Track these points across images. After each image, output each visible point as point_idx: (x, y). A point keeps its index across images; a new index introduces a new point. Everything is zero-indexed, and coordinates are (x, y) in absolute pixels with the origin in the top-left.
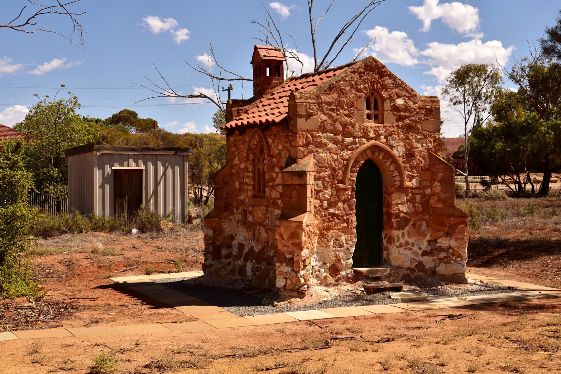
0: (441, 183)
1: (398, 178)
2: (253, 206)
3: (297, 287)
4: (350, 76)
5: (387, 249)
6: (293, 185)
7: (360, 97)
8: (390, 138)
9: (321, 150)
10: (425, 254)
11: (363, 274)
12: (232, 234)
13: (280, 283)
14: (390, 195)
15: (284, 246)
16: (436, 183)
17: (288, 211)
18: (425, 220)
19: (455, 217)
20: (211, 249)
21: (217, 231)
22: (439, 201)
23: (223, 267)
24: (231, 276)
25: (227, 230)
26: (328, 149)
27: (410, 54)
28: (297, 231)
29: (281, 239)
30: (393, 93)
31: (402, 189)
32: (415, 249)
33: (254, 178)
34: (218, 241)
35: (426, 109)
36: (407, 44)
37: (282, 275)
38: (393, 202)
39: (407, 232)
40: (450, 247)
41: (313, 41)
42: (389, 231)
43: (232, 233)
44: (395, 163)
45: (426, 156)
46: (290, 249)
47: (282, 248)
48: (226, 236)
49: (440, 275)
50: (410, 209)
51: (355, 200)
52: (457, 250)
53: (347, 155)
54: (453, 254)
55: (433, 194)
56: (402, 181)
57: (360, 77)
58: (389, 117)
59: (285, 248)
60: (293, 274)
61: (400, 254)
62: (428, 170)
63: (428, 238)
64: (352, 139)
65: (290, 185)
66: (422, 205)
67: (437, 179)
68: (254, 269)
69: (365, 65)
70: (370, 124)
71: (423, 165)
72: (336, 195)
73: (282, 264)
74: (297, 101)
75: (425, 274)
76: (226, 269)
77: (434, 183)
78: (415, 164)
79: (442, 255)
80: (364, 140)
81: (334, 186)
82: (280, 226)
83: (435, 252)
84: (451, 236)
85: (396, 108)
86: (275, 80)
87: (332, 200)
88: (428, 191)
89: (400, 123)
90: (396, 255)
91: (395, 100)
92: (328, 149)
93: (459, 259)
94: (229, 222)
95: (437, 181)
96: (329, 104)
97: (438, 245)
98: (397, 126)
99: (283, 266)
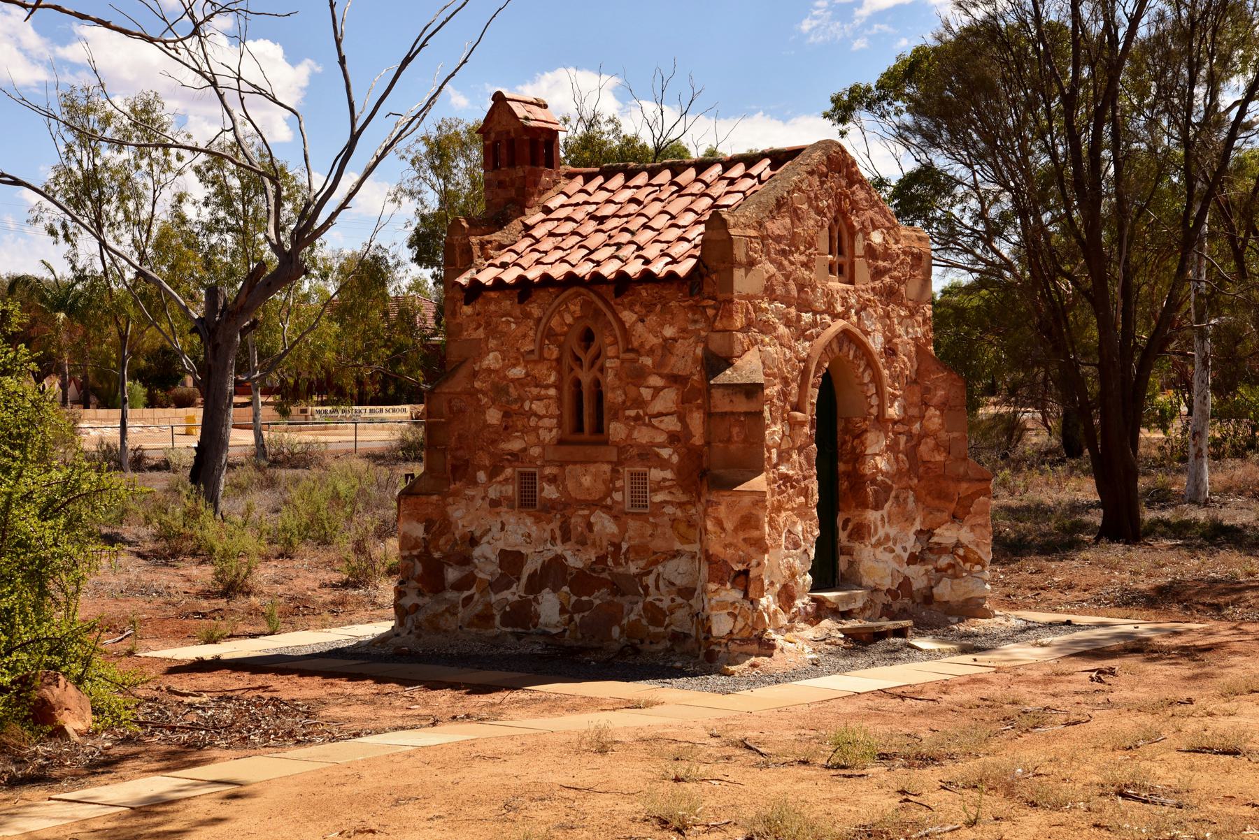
0: (942, 411)
1: (874, 401)
2: (562, 464)
3: (755, 633)
5: (849, 552)
6: (732, 413)
7: (822, 226)
8: (863, 314)
9: (767, 340)
10: (913, 559)
11: (827, 604)
12: (472, 532)
13: (721, 625)
14: (860, 435)
15: (726, 546)
16: (932, 411)
17: (722, 471)
18: (911, 488)
19: (970, 480)
20: (419, 569)
21: (437, 525)
22: (937, 447)
23: (447, 610)
24: (474, 630)
25: (460, 523)
26: (777, 338)
27: (25, 52)
28: (754, 512)
29: (719, 530)
32: (898, 549)
33: (559, 400)
34: (437, 549)
35: (912, 254)
36: (10, 19)
37: (726, 609)
38: (869, 451)
40: (958, 544)
41: (342, 61)
42: (857, 513)
43: (473, 529)
44: (872, 369)
45: (913, 354)
46: (741, 553)
47: (721, 549)
48: (457, 536)
49: (940, 603)
50: (891, 466)
51: (814, 445)
52: (974, 548)
53: (804, 349)
54: (965, 559)
56: (881, 408)
57: (822, 183)
58: (862, 269)
59: (730, 551)
60: (747, 604)
61: (876, 560)
62: (915, 382)
63: (917, 526)
65: (726, 413)
66: (906, 456)
67: (935, 401)
68: (569, 608)
69: (828, 157)
70: (835, 284)
71: (908, 372)
72: (790, 436)
73: (724, 584)
74: (732, 232)
75: (913, 603)
76: (456, 614)
77: (926, 410)
78: (898, 369)
79: (944, 561)
81: (785, 415)
82: (719, 504)
83: (930, 556)
84: (962, 520)
85: (871, 252)
86: (546, 176)
87: (784, 447)
88: (916, 427)
89: (878, 284)
90: (870, 564)
92: (777, 338)
93: (978, 568)
94: (467, 505)
95: (934, 407)
96: (778, 239)
97: (935, 539)
98: (873, 289)
99: (726, 590)
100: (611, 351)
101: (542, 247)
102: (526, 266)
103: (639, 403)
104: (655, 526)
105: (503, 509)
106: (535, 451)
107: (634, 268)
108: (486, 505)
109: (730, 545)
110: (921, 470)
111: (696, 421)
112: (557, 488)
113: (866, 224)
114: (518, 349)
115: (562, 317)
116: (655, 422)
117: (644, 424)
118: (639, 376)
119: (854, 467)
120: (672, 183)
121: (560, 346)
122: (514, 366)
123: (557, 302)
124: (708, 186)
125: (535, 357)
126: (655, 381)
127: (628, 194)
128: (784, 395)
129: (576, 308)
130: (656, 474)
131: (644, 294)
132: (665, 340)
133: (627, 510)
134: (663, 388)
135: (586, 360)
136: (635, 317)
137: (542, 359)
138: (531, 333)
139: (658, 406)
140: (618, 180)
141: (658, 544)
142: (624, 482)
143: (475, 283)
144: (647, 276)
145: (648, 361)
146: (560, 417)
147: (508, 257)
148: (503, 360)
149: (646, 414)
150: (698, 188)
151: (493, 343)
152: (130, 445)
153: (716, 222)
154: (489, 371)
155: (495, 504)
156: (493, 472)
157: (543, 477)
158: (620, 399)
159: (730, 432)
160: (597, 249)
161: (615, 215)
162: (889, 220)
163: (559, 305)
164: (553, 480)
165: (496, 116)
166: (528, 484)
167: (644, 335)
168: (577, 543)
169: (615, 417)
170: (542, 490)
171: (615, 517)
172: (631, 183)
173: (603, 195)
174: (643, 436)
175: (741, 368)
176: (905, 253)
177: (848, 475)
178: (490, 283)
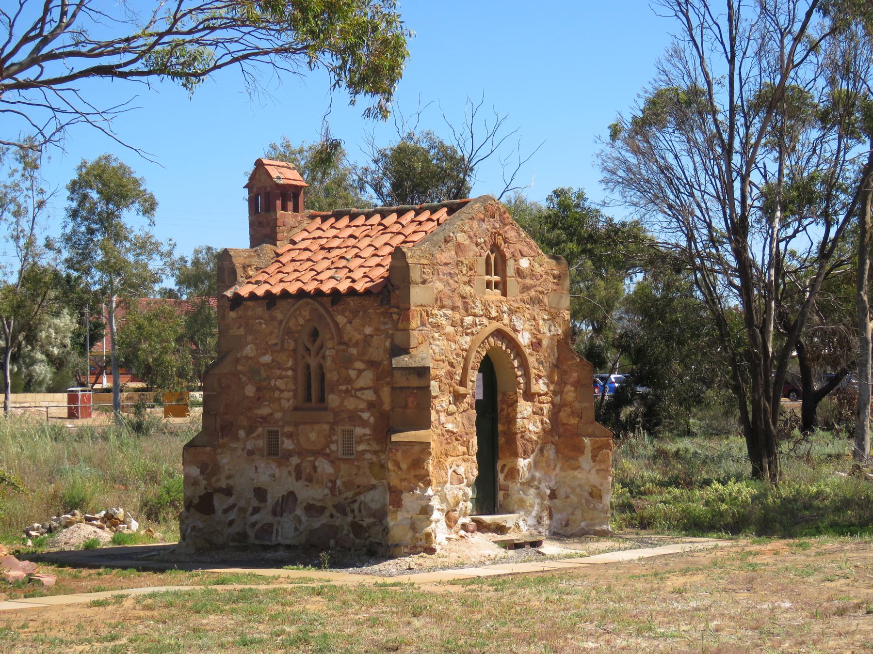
0: (576, 388)
2: (296, 425)
5: (506, 489)
6: (408, 388)
9: (436, 335)
15: (401, 480)
16: (569, 388)
22: (573, 413)
29: (396, 469)
31: (529, 396)
33: (295, 378)
43: (438, 551)
58: (513, 284)
67: (572, 380)
85: (519, 272)
89: (525, 296)
100: (329, 344)
101: (285, 270)
102: (273, 283)
103: (349, 381)
104: (359, 467)
105: (256, 457)
106: (278, 415)
107: (343, 287)
108: (245, 454)
109: (405, 479)
110: (561, 430)
111: (386, 392)
112: (293, 441)
113: (516, 254)
114: (267, 343)
115: (297, 320)
116: (359, 394)
117: (352, 396)
118: (347, 362)
119: (509, 428)
120: (380, 224)
121: (295, 341)
122: (264, 354)
123: (293, 309)
124: (403, 226)
125: (278, 348)
126: (359, 365)
127: (349, 231)
128: (451, 375)
129: (306, 314)
130: (359, 431)
131: (352, 304)
132: (366, 336)
133: (340, 456)
134: (364, 370)
135: (313, 350)
136: (345, 320)
137: (283, 349)
138: (276, 331)
139: (361, 383)
140: (345, 221)
141: (362, 480)
142: (338, 437)
143: (237, 296)
144: (352, 291)
145: (354, 351)
146: (295, 391)
147: (262, 277)
148: (257, 350)
149: (353, 389)
150: (397, 228)
151: (250, 338)
153: (398, 254)
154: (247, 358)
155: (251, 453)
156: (250, 431)
157: (284, 434)
158: (335, 378)
159: (407, 401)
160: (322, 272)
161: (338, 247)
162: (534, 251)
163: (295, 311)
164: (290, 436)
165: (257, 176)
166: (273, 438)
167: (352, 333)
168: (306, 480)
169: (332, 391)
170: (283, 443)
171: (332, 462)
172: (353, 224)
173: (334, 232)
174: (350, 404)
175: (415, 356)
176: (547, 274)
177: (505, 433)
178: (247, 295)
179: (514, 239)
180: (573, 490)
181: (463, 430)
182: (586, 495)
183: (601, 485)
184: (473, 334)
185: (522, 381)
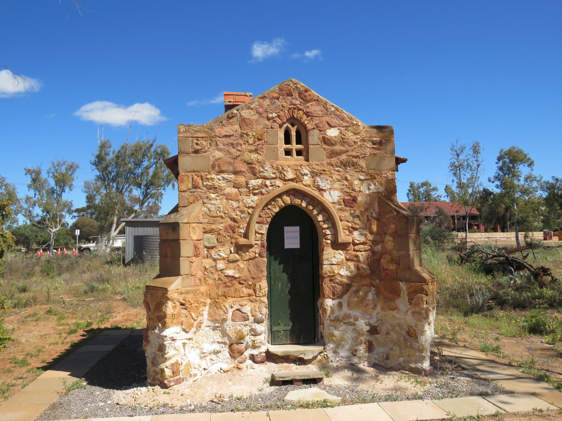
4: (257, 103)
9: (213, 196)
16: (388, 238)
18: (374, 286)
22: (392, 260)
30: (322, 122)
31: (337, 245)
39: (347, 302)
55: (384, 252)
64: (260, 181)
67: (390, 231)
77: (385, 237)
80: (278, 182)
85: (326, 141)
89: (334, 160)
91: (325, 130)
152: (502, 387)
179: (320, 113)
180: (393, 327)
181: (248, 275)
182: (404, 333)
183: (416, 326)
184: (262, 194)
185: (328, 232)
